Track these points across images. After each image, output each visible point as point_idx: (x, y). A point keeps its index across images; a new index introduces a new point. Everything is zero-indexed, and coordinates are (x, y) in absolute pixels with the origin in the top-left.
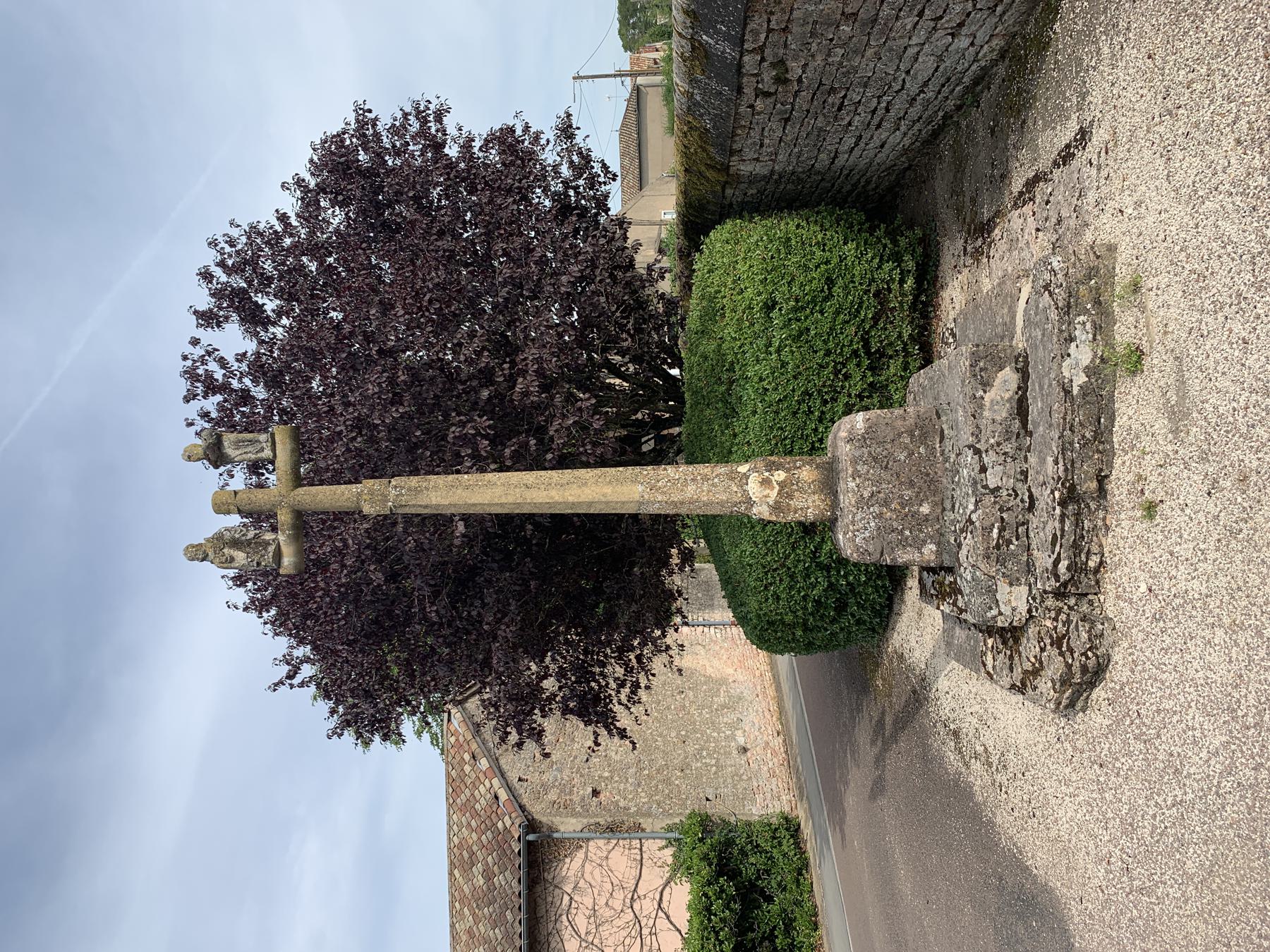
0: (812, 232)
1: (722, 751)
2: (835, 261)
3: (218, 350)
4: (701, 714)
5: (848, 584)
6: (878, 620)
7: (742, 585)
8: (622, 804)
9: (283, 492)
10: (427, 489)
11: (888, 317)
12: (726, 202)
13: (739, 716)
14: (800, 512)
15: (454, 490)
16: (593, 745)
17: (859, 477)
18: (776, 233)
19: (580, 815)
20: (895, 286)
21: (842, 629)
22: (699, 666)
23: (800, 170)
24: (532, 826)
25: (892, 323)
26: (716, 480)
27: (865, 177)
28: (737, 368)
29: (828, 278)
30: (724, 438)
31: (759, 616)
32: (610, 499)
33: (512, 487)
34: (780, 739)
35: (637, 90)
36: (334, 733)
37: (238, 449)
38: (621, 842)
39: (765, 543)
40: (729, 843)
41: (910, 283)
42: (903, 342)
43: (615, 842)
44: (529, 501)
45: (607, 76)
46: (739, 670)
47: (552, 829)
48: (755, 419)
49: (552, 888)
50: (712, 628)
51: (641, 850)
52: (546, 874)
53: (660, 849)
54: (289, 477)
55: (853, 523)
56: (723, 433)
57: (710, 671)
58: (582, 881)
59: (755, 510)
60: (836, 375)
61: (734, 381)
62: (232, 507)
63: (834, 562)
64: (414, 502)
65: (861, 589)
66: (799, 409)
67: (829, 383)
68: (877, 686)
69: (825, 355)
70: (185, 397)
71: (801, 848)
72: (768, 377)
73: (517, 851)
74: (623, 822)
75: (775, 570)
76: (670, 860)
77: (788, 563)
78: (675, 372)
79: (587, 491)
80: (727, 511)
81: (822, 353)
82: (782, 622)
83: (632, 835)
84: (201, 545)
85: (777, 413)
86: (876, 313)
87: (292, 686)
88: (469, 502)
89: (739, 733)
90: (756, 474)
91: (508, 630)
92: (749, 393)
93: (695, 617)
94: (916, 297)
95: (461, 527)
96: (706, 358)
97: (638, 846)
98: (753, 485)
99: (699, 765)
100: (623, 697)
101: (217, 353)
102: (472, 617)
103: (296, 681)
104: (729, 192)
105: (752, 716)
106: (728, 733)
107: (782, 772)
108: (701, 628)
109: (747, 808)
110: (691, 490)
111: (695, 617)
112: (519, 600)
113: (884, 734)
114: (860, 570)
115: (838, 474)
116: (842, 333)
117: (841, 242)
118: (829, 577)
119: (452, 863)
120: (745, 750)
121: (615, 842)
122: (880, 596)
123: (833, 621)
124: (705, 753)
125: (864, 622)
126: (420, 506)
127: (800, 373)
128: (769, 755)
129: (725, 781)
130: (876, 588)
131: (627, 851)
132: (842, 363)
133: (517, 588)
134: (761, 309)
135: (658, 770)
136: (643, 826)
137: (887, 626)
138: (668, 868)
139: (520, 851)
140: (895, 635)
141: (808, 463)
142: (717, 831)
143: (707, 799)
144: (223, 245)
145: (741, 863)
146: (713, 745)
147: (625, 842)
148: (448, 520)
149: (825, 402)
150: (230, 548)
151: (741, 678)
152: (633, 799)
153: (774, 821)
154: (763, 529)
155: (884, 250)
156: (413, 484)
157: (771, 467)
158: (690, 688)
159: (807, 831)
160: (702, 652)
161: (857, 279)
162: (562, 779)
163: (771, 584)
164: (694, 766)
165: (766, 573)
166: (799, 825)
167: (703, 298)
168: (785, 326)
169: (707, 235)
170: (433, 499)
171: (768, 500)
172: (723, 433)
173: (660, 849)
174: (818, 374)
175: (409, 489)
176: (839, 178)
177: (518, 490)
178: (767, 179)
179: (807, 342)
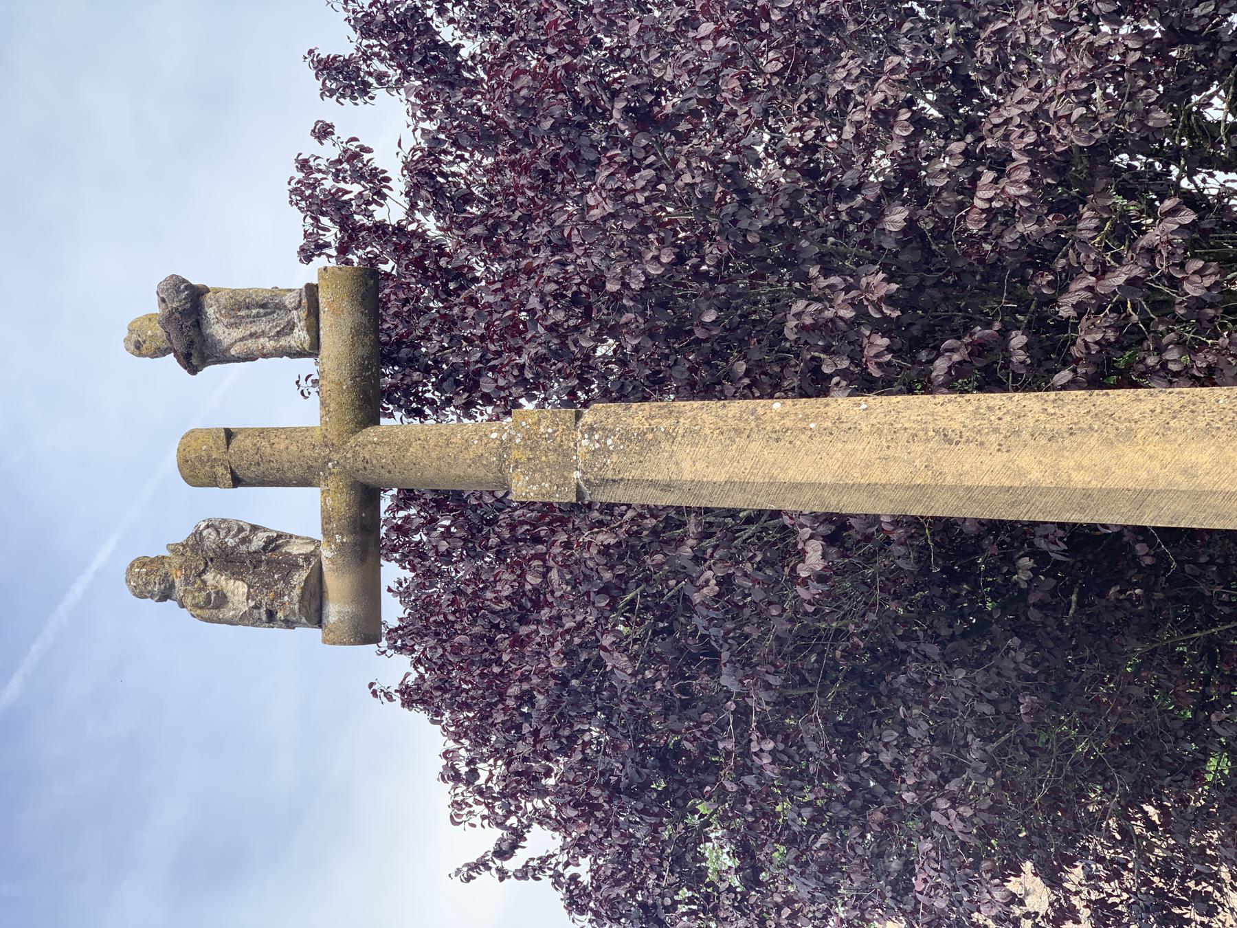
3: (369, 151)
9: (332, 436)
15: (741, 441)
32: (1207, 483)
44: (949, 480)
54: (346, 398)
62: (220, 471)
64: (636, 473)
70: (302, 250)
79: (1131, 455)
84: (161, 560)
87: (503, 875)
88: (782, 477)
91: (952, 813)
95: (814, 557)
101: (366, 157)
112: (990, 740)
126: (652, 484)
133: (987, 709)
150: (220, 570)
156: (635, 423)
170: (686, 465)
175: (626, 437)
177: (918, 448)
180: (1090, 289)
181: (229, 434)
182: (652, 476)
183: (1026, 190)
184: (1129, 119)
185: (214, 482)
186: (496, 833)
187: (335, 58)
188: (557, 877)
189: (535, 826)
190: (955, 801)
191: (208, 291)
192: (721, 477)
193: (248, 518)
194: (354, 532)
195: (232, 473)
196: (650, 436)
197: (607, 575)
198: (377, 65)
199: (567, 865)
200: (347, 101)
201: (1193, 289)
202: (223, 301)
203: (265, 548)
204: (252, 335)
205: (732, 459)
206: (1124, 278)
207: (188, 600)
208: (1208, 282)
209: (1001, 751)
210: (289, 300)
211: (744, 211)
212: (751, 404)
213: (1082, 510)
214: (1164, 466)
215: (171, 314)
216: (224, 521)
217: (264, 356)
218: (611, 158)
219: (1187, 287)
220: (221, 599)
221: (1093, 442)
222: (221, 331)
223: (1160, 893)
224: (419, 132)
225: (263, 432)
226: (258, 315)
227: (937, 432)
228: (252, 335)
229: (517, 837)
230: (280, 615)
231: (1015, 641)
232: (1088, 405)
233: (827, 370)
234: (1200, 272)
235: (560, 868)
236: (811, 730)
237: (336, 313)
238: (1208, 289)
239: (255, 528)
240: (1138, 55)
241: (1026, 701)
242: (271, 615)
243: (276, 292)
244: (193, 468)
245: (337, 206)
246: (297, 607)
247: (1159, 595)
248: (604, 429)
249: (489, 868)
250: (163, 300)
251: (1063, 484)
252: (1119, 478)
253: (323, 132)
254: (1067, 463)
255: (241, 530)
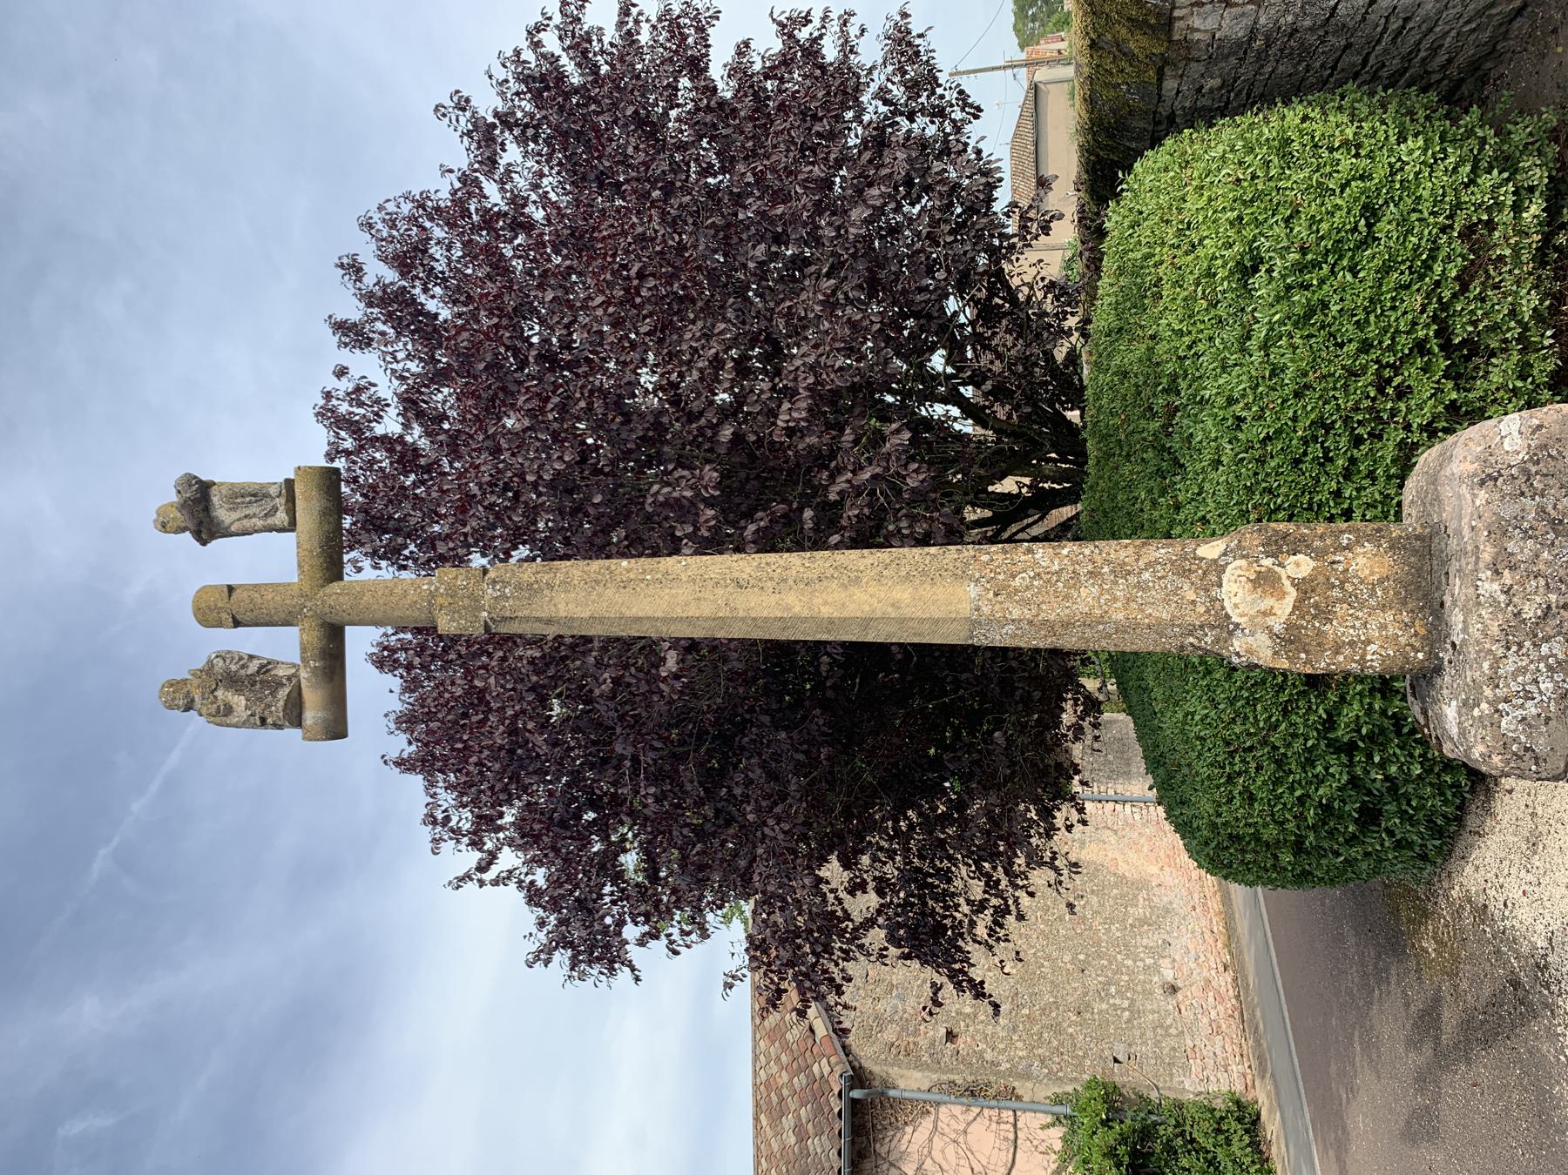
0: (1334, 125)
1: (1139, 988)
2: (1380, 173)
3: (375, 385)
4: (1108, 930)
5: (1387, 778)
6: (1438, 843)
7: (1185, 770)
8: (989, 1056)
9: (306, 589)
10: (550, 586)
11: (1488, 276)
12: (1164, 111)
13: (1166, 936)
14: (1347, 651)
16: (930, 1004)
17: (1513, 568)
18: (1261, 134)
19: (928, 1067)
20: (1506, 216)
21: (1367, 854)
22: (1108, 859)
23: (1308, 23)
24: (858, 1077)
25: (1496, 287)
26: (1146, 575)
27: (1431, 38)
28: (1183, 385)
29: (1365, 207)
30: (1156, 513)
31: (1214, 826)
32: (907, 612)
33: (710, 584)
34: (1229, 977)
35: (1035, 89)
36: (537, 958)
37: (234, 509)
38: (986, 1111)
39: (1232, 701)
40: (1146, 1133)
41: (1534, 209)
42: (1519, 322)
43: (977, 1110)
44: (741, 614)
45: (993, 69)
46: (1167, 869)
47: (888, 1084)
48: (1220, 475)
49: (885, 1166)
50: (1128, 806)
51: (1015, 1125)
52: (878, 1146)
53: (1043, 1127)
54: (317, 562)
55: (1494, 681)
56: (1154, 504)
57: (1123, 868)
58: (929, 1161)
59: (1237, 644)
60: (1381, 390)
61: (1177, 409)
62: (224, 616)
63: (1362, 739)
64: (527, 613)
65: (1410, 788)
66: (1305, 454)
67: (1366, 403)
68: (1425, 950)
69: (1360, 351)
71: (1261, 1152)
72: (1243, 396)
73: (836, 1110)
74: (989, 1084)
75: (1251, 749)
76: (1058, 1145)
77: (1275, 738)
78: (1073, 415)
79: (858, 594)
80: (1169, 644)
81: (1353, 346)
82: (1257, 837)
83: (1002, 1104)
85: (1261, 461)
86: (1464, 270)
87: (482, 883)
88: (628, 613)
89: (1165, 963)
90: (1243, 562)
92: (1205, 428)
93: (1103, 788)
94: (1547, 239)
96: (1125, 375)
97: (1011, 1120)
98: (1235, 587)
99: (1104, 1006)
100: (981, 931)
101: (373, 389)
102: (734, 796)
103: (489, 876)
104: (1170, 85)
105: (1186, 939)
106: (1149, 961)
107: (1232, 1028)
108: (1111, 805)
109: (1176, 1079)
110: (1087, 597)
111: (1103, 788)
113: (1438, 1038)
114: (1411, 756)
115: (1445, 562)
116: (1394, 308)
117: (1393, 139)
118: (1351, 764)
119: (757, 1105)
120: (1174, 989)
121: (977, 1110)
122: (1446, 802)
123: (1352, 840)
124: (1113, 990)
125: (1410, 845)
126: (539, 620)
127: (1307, 387)
128: (1211, 999)
129: (1142, 1035)
130: (1440, 789)
131: (994, 1126)
132: (1392, 366)
133: (801, 757)
134: (1232, 273)
135: (1043, 1010)
136: (1019, 1092)
137: (1450, 852)
138: (1054, 1157)
139: (840, 1111)
140: (1469, 869)
141: (1369, 538)
142: (1130, 1114)
143: (1116, 1060)
144: (380, 226)
145: (1166, 1165)
146: (1127, 978)
147: (992, 1112)
148: (649, 648)
149: (1357, 441)
150: (227, 688)
151: (1169, 881)
152: (1005, 1050)
153: (1219, 1104)
154: (1229, 677)
155: (1481, 150)
156: (525, 577)
157: (1278, 547)
158: (1093, 892)
159: (1272, 1126)
160: (1113, 839)
161: (1425, 207)
162: (905, 1011)
163: (1239, 774)
164: (1097, 1007)
165: (1231, 754)
166: (1258, 1115)
167: (1121, 271)
168: (1278, 299)
169: (1129, 168)
170: (561, 606)
171: (1270, 621)
172: (1154, 504)
173: (1043, 1127)
174: (1346, 386)
175: (519, 587)
176: (1379, 42)
177: (720, 591)
178: (1241, 48)
179: (1323, 327)
180: (848, 481)
181: (231, 589)
182: (538, 614)
183: (804, 414)
184: (876, 369)
185: (220, 624)
186: (477, 855)
187: (346, 321)
188: (520, 882)
189: (506, 848)
190: (779, 820)
191: (214, 484)
192: (586, 615)
193: (247, 650)
194: (324, 659)
195: (233, 617)
196: (536, 586)
197: (534, 678)
198: (379, 326)
199: (527, 874)
200: (357, 351)
201: (912, 482)
202: (224, 492)
203: (258, 672)
204: (246, 517)
205: (594, 601)
206: (869, 474)
207: (204, 711)
208: (921, 477)
209: (812, 783)
210: (273, 491)
211: (625, 427)
212: (607, 562)
213: (829, 632)
214: (879, 602)
215: (185, 502)
216: (229, 652)
217: (256, 532)
218: (527, 388)
219: (909, 481)
220: (229, 710)
221: (834, 586)
222: (223, 514)
223: (918, 870)
224: (389, 372)
225: (256, 587)
226: (250, 502)
227: (732, 580)
228: (246, 517)
229: (492, 857)
230: (269, 721)
231: (817, 712)
232: (831, 560)
233: (678, 534)
234: (917, 471)
235: (522, 877)
236: (689, 773)
237: (307, 499)
238: (922, 482)
239: (251, 657)
240: (879, 325)
241: (824, 751)
242: (263, 721)
243: (262, 486)
244: (204, 614)
245: (355, 428)
246: (281, 714)
247: (909, 678)
248: (503, 582)
249: (472, 880)
250: (179, 492)
251: (815, 615)
252: (852, 611)
253: (341, 372)
254: (818, 601)
255: (241, 658)
